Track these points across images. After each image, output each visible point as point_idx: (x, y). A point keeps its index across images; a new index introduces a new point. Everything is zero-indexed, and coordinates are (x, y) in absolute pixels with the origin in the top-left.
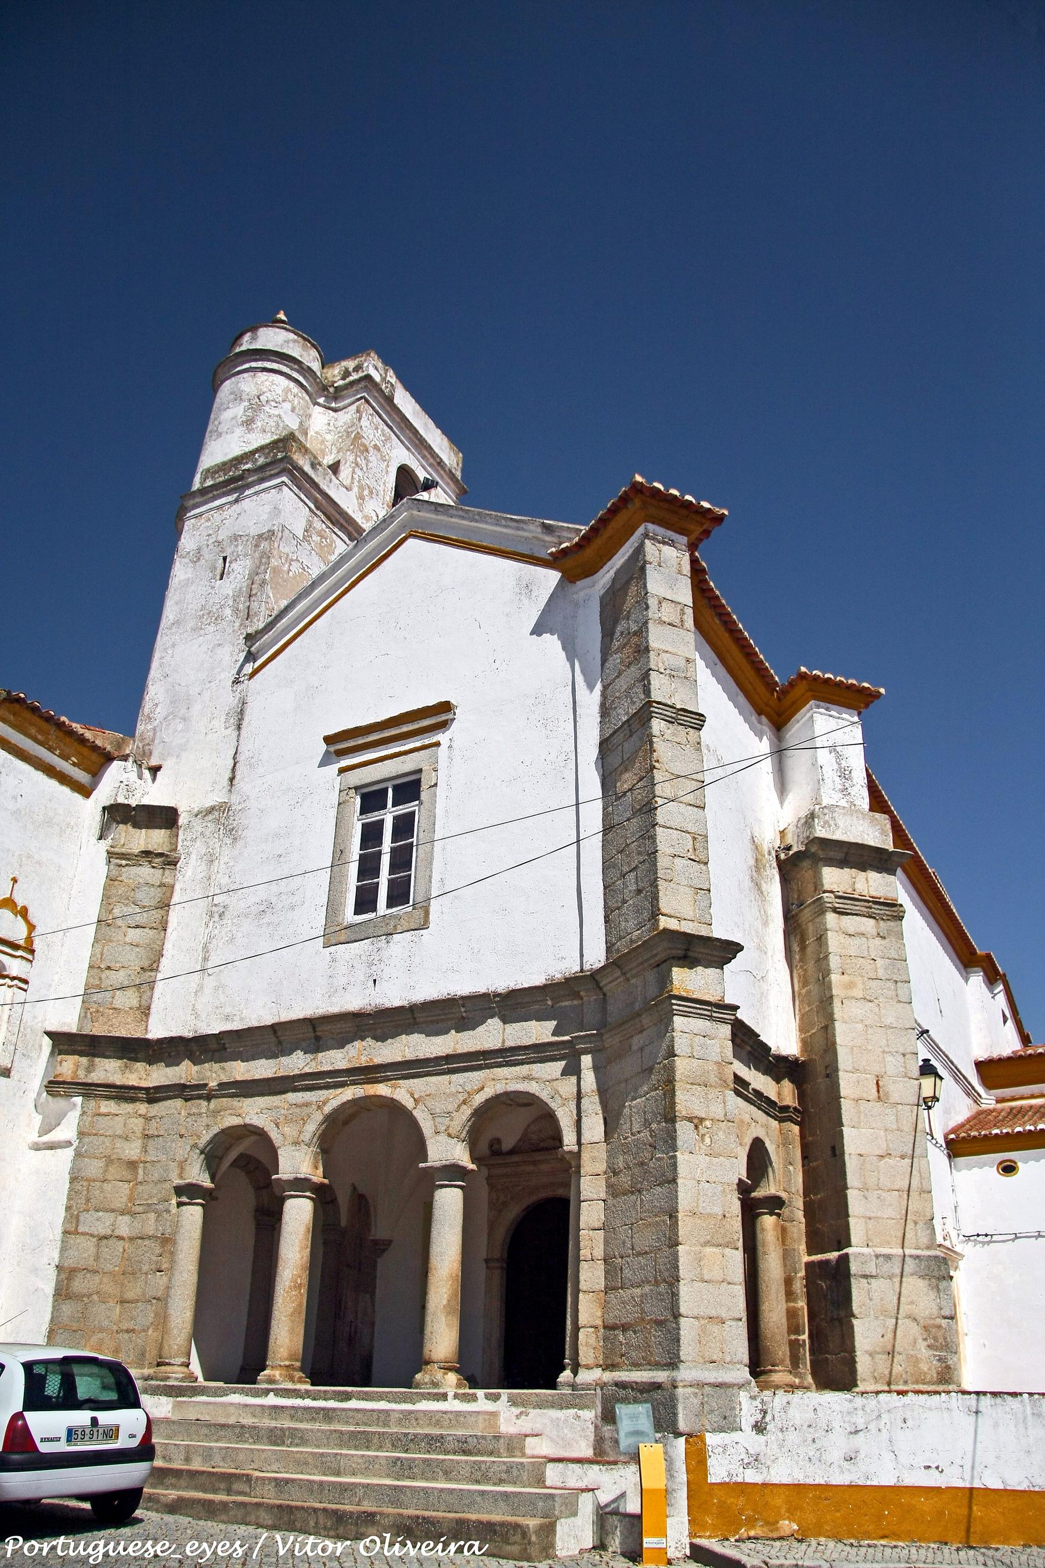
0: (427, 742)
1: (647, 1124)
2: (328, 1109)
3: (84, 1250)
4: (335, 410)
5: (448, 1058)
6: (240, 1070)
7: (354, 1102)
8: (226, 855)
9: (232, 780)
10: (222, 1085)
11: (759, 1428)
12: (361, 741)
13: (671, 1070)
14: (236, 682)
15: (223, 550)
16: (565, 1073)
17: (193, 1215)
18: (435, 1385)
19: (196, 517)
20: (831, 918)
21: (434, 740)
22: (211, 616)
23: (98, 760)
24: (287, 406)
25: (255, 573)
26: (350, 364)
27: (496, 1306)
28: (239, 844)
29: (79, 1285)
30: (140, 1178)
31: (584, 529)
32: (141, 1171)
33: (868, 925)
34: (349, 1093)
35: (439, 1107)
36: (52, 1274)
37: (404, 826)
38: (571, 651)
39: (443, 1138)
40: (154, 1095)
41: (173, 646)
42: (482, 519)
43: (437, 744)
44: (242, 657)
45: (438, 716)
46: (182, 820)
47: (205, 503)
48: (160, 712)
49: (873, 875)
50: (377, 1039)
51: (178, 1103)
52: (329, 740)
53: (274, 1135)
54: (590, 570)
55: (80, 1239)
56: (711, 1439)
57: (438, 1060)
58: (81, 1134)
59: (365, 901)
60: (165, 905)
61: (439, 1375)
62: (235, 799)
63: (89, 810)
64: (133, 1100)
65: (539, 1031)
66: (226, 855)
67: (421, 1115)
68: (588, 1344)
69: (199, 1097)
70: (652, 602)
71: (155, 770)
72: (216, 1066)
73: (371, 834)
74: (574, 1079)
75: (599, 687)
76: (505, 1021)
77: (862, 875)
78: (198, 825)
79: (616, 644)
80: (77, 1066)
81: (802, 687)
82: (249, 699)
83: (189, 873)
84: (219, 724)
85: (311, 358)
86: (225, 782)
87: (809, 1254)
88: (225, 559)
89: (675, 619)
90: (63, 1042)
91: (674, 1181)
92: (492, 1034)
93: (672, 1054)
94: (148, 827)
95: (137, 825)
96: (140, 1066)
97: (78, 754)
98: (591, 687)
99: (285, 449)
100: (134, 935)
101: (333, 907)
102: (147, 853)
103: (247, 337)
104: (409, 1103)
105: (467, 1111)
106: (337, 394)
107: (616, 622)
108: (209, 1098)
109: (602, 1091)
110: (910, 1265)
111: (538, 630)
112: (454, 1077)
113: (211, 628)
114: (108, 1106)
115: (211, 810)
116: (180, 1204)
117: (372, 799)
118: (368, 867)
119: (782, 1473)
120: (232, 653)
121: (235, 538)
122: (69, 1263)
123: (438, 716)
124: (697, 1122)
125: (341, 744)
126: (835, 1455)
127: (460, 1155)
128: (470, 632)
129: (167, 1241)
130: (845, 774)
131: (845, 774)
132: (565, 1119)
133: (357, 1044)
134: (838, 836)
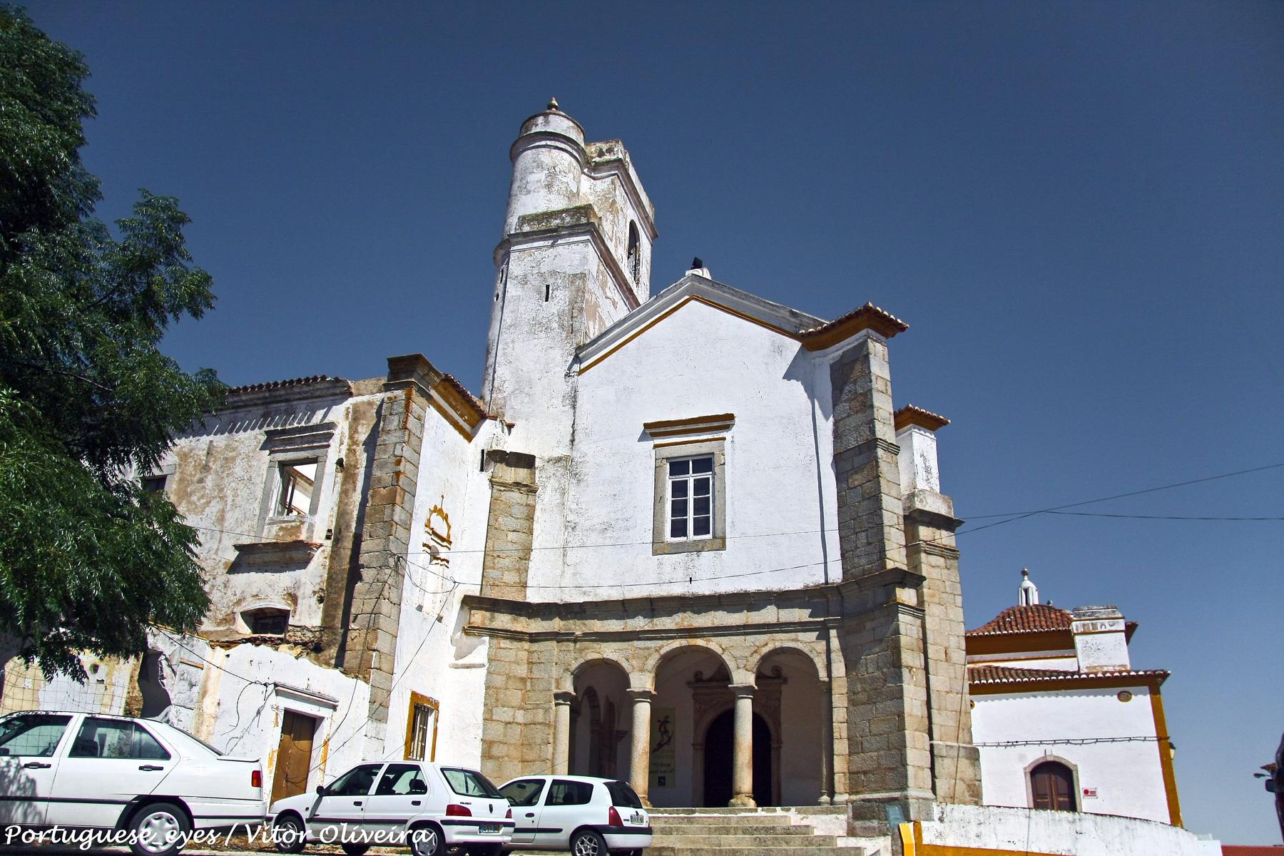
0: (716, 436)
1: (879, 668)
2: (663, 651)
3: (497, 731)
4: (594, 179)
5: (745, 626)
6: (597, 626)
7: (681, 648)
8: (573, 490)
9: (572, 441)
10: (585, 634)
11: (941, 820)
12: (669, 429)
13: (898, 642)
14: (568, 375)
15: (545, 280)
16: (818, 638)
17: (565, 711)
18: (744, 804)
19: (519, 251)
20: (923, 555)
21: (721, 435)
22: (539, 326)
23: (477, 417)
24: (571, 175)
25: (573, 303)
26: (605, 147)
27: (701, 777)
28: (582, 484)
29: (496, 751)
30: (529, 688)
31: (827, 323)
32: (528, 684)
33: (940, 561)
34: (676, 644)
35: (738, 654)
36: (479, 745)
37: (702, 486)
38: (812, 395)
39: (742, 671)
40: (534, 638)
41: (513, 342)
42: (747, 297)
43: (724, 439)
44: (571, 359)
45: (724, 422)
46: (538, 463)
47: (526, 242)
48: (508, 387)
49: (944, 533)
50: (695, 612)
51: (554, 643)
52: (646, 426)
53: (625, 665)
54: (823, 346)
55: (494, 724)
56: (924, 824)
57: (738, 627)
58: (490, 660)
59: (679, 529)
60: (530, 518)
61: (746, 800)
62: (575, 454)
63: (472, 451)
64: (521, 640)
65: (802, 615)
66: (573, 490)
67: (725, 657)
68: (840, 782)
69: (568, 640)
70: (873, 378)
71: (510, 427)
72: (578, 622)
73: (679, 489)
74: (824, 643)
75: (831, 419)
76: (779, 607)
77: (938, 532)
78: (550, 469)
79: (844, 397)
80: (484, 618)
81: (908, 414)
82: (580, 389)
83: (546, 498)
84: (558, 401)
85: (575, 135)
86: (568, 443)
87: (591, 787)
88: (548, 287)
89: (883, 389)
90: (469, 602)
91: (901, 698)
92: (770, 614)
93: (897, 632)
94: (516, 466)
95: (508, 465)
96: (523, 619)
97: (470, 415)
98: (827, 419)
99: (587, 216)
100: (512, 536)
101: (657, 531)
102: (517, 484)
103: (540, 120)
104: (719, 651)
105: (757, 657)
106: (596, 167)
107: (845, 383)
108: (575, 641)
109: (844, 649)
110: (962, 752)
111: (788, 376)
112: (748, 637)
113: (542, 335)
114: (505, 643)
115: (559, 460)
116: (557, 705)
117: (678, 467)
118: (679, 508)
119: (951, 842)
120: (560, 357)
121: (554, 273)
122: (488, 738)
123: (724, 422)
124: (910, 668)
125: (653, 430)
126: (972, 835)
127: (750, 679)
128: (728, 362)
129: (553, 726)
130: (928, 470)
131: (928, 470)
132: (820, 663)
133: (680, 614)
134: (927, 508)
